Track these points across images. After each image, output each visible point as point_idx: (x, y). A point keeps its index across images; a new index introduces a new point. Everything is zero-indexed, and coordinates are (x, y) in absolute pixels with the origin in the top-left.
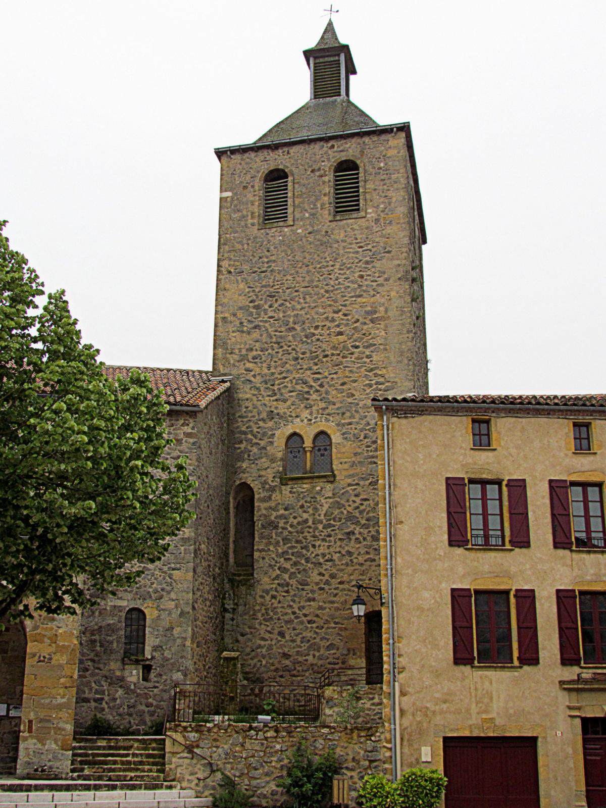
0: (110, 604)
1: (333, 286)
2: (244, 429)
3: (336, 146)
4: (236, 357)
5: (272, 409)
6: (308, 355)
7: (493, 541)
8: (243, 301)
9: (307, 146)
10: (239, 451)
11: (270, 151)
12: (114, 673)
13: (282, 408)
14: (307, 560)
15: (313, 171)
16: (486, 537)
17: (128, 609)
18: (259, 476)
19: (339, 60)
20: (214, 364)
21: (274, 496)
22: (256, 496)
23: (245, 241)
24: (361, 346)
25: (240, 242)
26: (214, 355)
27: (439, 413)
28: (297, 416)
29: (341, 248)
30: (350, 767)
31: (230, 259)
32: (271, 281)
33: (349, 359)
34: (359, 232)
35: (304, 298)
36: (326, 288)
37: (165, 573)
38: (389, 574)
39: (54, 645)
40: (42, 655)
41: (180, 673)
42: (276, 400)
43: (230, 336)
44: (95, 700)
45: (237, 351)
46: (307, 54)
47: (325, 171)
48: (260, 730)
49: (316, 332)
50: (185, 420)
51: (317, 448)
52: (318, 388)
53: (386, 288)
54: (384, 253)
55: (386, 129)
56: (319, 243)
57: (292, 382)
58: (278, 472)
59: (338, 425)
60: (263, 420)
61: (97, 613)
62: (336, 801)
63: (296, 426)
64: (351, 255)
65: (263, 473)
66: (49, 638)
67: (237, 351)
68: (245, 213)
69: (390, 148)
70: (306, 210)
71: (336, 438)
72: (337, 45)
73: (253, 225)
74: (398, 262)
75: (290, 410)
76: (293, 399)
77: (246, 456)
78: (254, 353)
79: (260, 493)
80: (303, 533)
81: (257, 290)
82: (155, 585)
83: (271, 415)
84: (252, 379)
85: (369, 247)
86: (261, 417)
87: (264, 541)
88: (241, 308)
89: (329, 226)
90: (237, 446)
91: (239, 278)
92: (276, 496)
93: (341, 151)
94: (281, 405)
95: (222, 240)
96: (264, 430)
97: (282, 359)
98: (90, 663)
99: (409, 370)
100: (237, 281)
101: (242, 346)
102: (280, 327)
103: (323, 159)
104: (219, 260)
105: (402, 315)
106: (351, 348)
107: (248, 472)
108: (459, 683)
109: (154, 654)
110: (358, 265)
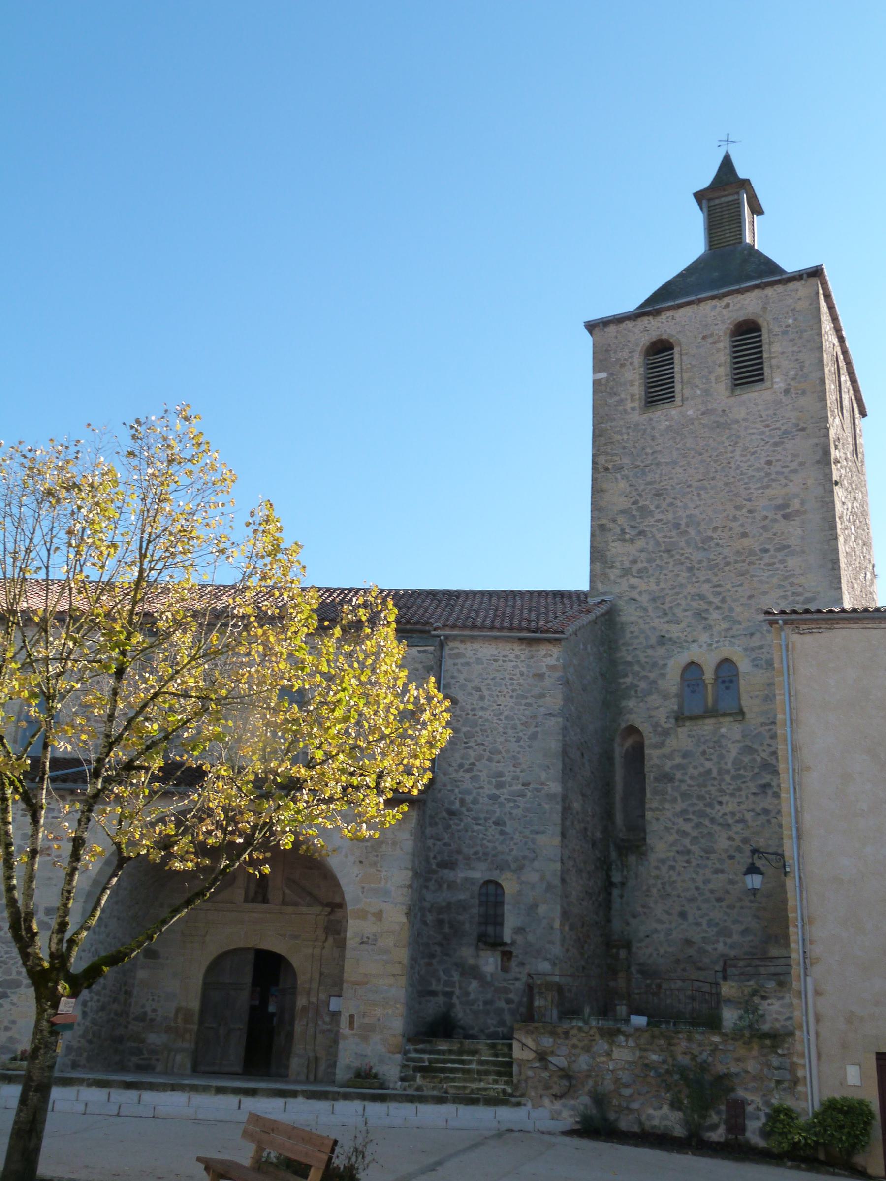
1: (734, 477)
2: (629, 659)
3: (731, 305)
4: (617, 572)
5: (663, 634)
6: (705, 564)
13: (675, 631)
20: (592, 581)
21: (668, 741)
22: (647, 742)
23: (624, 430)
24: (772, 550)
28: (694, 641)
31: (607, 454)
32: (657, 476)
35: (699, 495)
38: (794, 835)
42: (668, 622)
46: (699, 196)
49: (714, 535)
51: (720, 680)
59: (746, 649)
60: (652, 647)
61: (445, 886)
63: (694, 653)
66: (374, 914)
67: (618, 565)
68: (623, 396)
70: (697, 386)
71: (744, 665)
73: (633, 409)
75: (685, 634)
78: (640, 565)
79: (650, 739)
81: (640, 489)
83: (662, 640)
85: (778, 425)
87: (657, 797)
88: (622, 512)
91: (619, 476)
92: (672, 743)
93: (737, 310)
97: (673, 571)
100: (616, 479)
103: (715, 322)
106: (758, 552)
110: (765, 448)
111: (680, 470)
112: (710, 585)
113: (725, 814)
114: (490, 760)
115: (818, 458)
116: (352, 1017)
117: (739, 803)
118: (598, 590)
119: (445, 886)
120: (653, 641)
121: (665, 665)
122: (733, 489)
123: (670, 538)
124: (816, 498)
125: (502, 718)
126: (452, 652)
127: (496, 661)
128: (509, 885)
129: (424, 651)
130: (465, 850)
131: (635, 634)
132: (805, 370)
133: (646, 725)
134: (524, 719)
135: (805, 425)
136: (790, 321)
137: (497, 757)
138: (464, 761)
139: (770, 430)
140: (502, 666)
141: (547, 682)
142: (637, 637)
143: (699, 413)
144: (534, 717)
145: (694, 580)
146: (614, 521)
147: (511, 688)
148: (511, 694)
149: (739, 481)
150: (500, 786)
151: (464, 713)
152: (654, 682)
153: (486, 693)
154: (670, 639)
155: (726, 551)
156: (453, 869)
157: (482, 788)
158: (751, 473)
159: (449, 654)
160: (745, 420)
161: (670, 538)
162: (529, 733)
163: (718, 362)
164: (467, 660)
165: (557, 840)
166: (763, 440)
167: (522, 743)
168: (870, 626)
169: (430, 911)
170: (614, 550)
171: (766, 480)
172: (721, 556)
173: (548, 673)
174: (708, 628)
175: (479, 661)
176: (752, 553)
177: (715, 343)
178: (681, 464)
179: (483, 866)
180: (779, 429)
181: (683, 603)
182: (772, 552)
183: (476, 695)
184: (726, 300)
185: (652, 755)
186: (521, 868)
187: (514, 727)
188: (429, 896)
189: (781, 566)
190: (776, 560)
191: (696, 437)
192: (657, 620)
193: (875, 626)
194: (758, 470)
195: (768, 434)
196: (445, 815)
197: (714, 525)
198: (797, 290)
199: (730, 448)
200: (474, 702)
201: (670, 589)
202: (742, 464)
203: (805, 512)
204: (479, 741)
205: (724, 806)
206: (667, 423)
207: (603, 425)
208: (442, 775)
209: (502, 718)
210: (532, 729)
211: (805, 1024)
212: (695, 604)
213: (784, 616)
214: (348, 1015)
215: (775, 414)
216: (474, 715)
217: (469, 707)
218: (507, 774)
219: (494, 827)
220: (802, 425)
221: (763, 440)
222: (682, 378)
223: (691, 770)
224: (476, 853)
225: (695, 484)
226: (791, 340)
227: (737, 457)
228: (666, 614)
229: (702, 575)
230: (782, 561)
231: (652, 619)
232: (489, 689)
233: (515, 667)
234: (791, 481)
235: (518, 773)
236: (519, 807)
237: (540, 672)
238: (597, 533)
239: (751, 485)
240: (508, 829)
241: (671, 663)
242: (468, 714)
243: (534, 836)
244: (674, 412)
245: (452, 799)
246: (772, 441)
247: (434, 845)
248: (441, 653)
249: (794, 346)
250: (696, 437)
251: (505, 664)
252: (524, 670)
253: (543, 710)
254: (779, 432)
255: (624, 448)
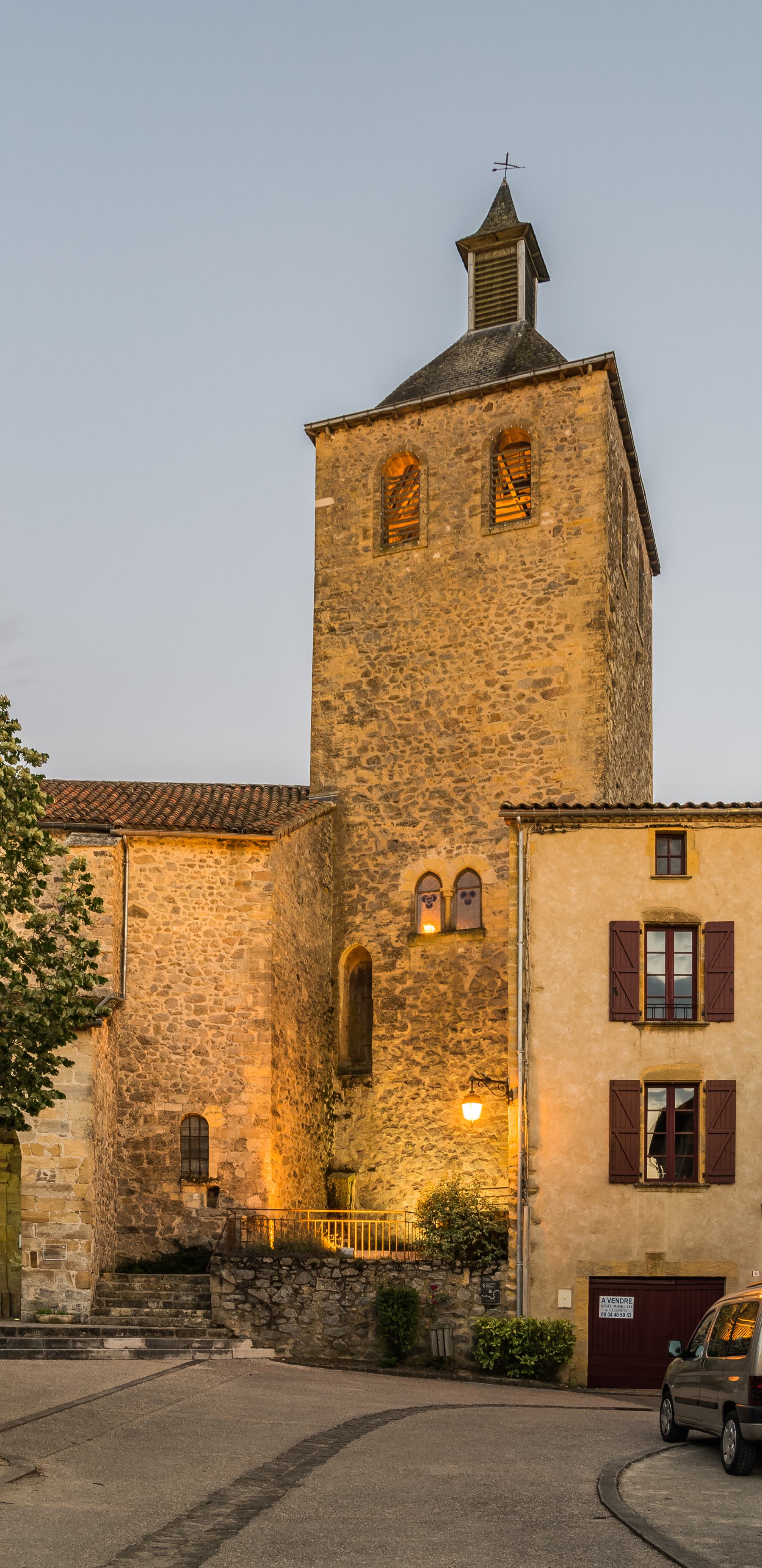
0: (159, 1108)
1: (486, 643)
2: (356, 867)
3: (495, 406)
4: (344, 762)
5: (396, 838)
6: (447, 754)
7: (679, 1014)
8: (354, 675)
9: (449, 409)
10: (350, 900)
11: (391, 423)
12: (169, 1196)
13: (409, 835)
14: (445, 1048)
15: (459, 452)
16: (670, 1007)
17: (183, 1115)
18: (379, 935)
19: (515, 255)
20: (313, 773)
21: (399, 962)
22: (375, 964)
23: (354, 578)
24: (527, 736)
25: (346, 581)
26: (313, 760)
27: (605, 825)
28: (431, 847)
29: (499, 579)
30: (459, 1313)
31: (333, 609)
32: (394, 639)
33: (508, 757)
34: (528, 551)
35: (443, 665)
36: (476, 646)
37: (233, 1067)
38: (520, 1061)
39: (56, 1159)
40: (42, 1171)
41: (257, 1197)
42: (402, 824)
43: (334, 731)
44: (146, 1231)
45: (345, 752)
46: (463, 247)
47: (477, 452)
48: (335, 1267)
49: (460, 718)
50: (253, 854)
51: (460, 892)
52: (462, 803)
53: (569, 640)
54: (566, 584)
55: (576, 368)
56: (466, 573)
57: (424, 796)
58: (404, 928)
59: (491, 857)
60: (383, 853)
61: (141, 1120)
62: (435, 1354)
63: (432, 861)
64: (516, 590)
65: (382, 931)
66: (49, 1150)
67: (345, 752)
68: (353, 530)
69: (581, 401)
70: (446, 520)
71: (488, 876)
72: (509, 224)
73: (366, 549)
74: (588, 598)
75: (422, 838)
76: (425, 822)
77: (359, 907)
78: (371, 754)
79: (379, 959)
80: (439, 1012)
81: (373, 656)
82: (219, 1084)
83: (395, 845)
84: (368, 794)
85: (544, 575)
86: (380, 849)
87: (385, 1025)
88: (348, 686)
89: (482, 544)
90: (346, 893)
91: (346, 638)
92: (403, 964)
93: (501, 414)
94: (408, 830)
95: (320, 577)
96: (385, 869)
97: (409, 762)
98: (136, 1185)
99: (597, 770)
100: (344, 643)
101: (353, 744)
102: (408, 711)
103: (473, 431)
104: (316, 611)
105: (590, 683)
106: (511, 739)
107: (363, 930)
108: (615, 1208)
109: (221, 1172)
110: (526, 606)
111: (421, 632)
112: (453, 779)
113: (459, 1042)
114: (187, 982)
115: (589, 620)
116: (33, 1254)
117: (475, 1031)
118: (321, 785)
119: (141, 1120)
120: (384, 845)
121: (397, 875)
122: (485, 659)
123: (408, 720)
124: (583, 672)
125: (201, 933)
126: (137, 855)
127: (191, 866)
128: (214, 1117)
129: (103, 853)
130: (163, 1082)
131: (364, 838)
132: (582, 501)
133: (374, 944)
134: (226, 935)
135: (576, 577)
136: (568, 433)
137: (194, 979)
138: (157, 984)
139: (534, 582)
140: (199, 872)
141: (254, 892)
142: (366, 842)
143: (448, 556)
144: (238, 933)
145: (434, 772)
146: (341, 696)
147: (210, 898)
148: (211, 905)
149: (492, 648)
150: (200, 1011)
151: (155, 928)
152: (384, 895)
153: (180, 904)
154: (404, 844)
155: (473, 738)
156: (149, 1102)
157: (181, 1014)
158: (507, 638)
159: (134, 858)
160: (505, 568)
161: (408, 720)
162: (232, 951)
163: (474, 488)
164: (157, 865)
165: (267, 1070)
166: (524, 595)
167: (224, 963)
168: (622, 825)
169: (125, 1147)
170: (339, 735)
171: (525, 647)
172: (467, 744)
173: (254, 882)
174: (448, 831)
175: (170, 866)
176: (504, 740)
177: (470, 460)
178: (423, 624)
179: (184, 1099)
180: (544, 580)
181: (421, 800)
182: (527, 740)
183: (170, 907)
184: (488, 400)
185: (381, 978)
186: (226, 1101)
187: (214, 945)
188: (124, 1132)
189: (536, 758)
190: (531, 750)
191: (442, 589)
192: (389, 822)
193: (628, 825)
194: (517, 635)
195: (530, 587)
196: (137, 1043)
197: (461, 704)
198: (579, 388)
199: (485, 605)
200: (167, 915)
201: (405, 784)
202: (497, 626)
203: (568, 690)
204: (174, 960)
205: (458, 1033)
206: (408, 569)
207: (329, 571)
208: (133, 1000)
209: (201, 933)
210: (237, 947)
211: (518, 1253)
212: (435, 803)
213: (523, 812)
214: (29, 1252)
215: (540, 561)
216: (168, 930)
217: (160, 920)
218: (208, 998)
219: (194, 1056)
220: (573, 576)
221: (524, 595)
222: (428, 508)
223: (423, 994)
224: (175, 1085)
225: (439, 652)
226: (567, 460)
227: (491, 618)
228: (399, 814)
229: (443, 767)
230: (539, 752)
231: (383, 819)
232: (184, 900)
233: (215, 874)
234: (555, 650)
235: (221, 997)
236: (223, 1035)
237: (245, 880)
238: (320, 712)
239: (507, 654)
240: (211, 1059)
241: (404, 873)
242: (159, 929)
243: (240, 1066)
244: (416, 555)
245: (145, 1025)
246: (535, 597)
247: (127, 1076)
248: (125, 856)
249: (569, 468)
250: (442, 589)
251: (202, 870)
252: (226, 877)
253: (248, 925)
254: (544, 585)
255: (354, 602)
